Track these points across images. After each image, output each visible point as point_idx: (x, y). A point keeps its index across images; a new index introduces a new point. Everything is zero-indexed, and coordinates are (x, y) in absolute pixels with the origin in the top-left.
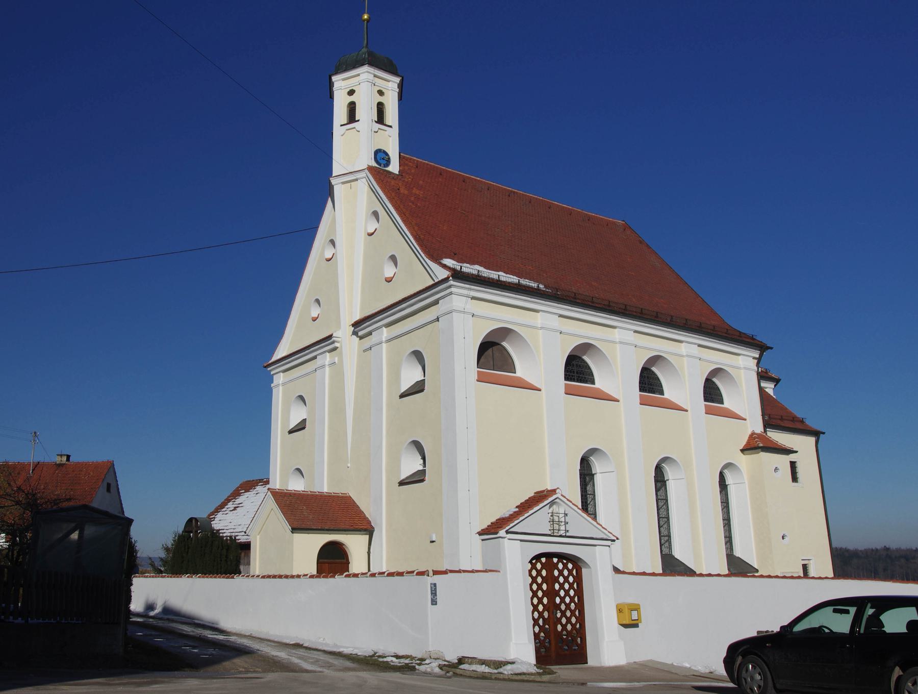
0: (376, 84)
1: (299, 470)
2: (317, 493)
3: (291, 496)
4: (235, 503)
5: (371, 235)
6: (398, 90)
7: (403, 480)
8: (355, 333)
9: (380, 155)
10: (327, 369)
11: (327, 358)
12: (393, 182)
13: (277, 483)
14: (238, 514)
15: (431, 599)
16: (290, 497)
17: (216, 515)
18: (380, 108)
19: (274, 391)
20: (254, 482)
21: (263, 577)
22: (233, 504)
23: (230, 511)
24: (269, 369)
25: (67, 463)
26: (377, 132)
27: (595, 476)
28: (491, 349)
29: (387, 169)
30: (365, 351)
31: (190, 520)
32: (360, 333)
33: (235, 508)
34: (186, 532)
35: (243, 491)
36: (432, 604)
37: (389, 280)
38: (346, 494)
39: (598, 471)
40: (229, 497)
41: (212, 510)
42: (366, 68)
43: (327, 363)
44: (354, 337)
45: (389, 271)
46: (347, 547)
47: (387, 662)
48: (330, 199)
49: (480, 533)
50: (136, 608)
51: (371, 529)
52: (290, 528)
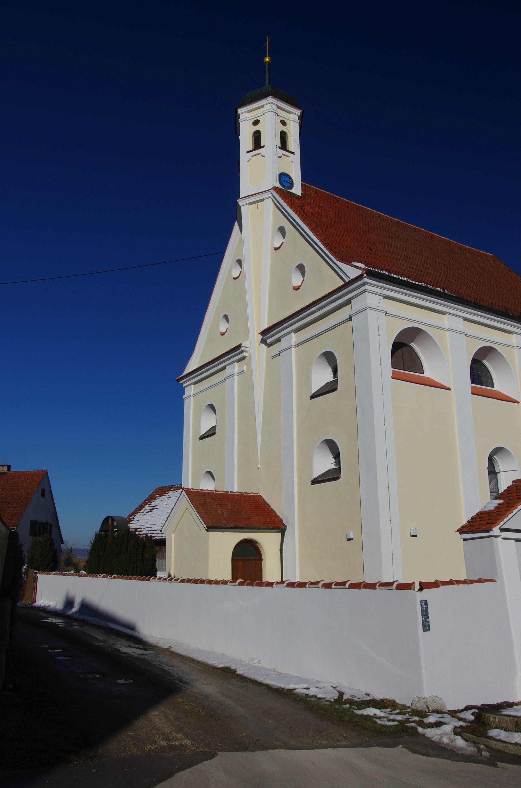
0: (279, 115)
1: (209, 473)
2: (230, 493)
3: (204, 495)
4: (151, 506)
5: (276, 249)
6: (298, 121)
7: (316, 478)
8: (263, 341)
9: (283, 178)
10: (236, 378)
11: (236, 368)
12: (297, 201)
13: (189, 483)
14: (153, 515)
15: (423, 622)
16: (204, 497)
17: (135, 516)
18: (283, 136)
19: (186, 402)
20: (166, 488)
21: (183, 581)
22: (149, 506)
23: (147, 512)
24: (181, 382)
25: (8, 472)
26: (280, 157)
27: (498, 475)
28: (401, 349)
29: (290, 191)
30: (273, 357)
31: (107, 519)
32: (268, 341)
33: (151, 510)
34: (104, 531)
35: (158, 496)
36: (424, 630)
37: (296, 288)
38: (257, 494)
39: (501, 470)
40: (145, 500)
41: (132, 511)
42: (270, 99)
43: (236, 372)
44: (263, 345)
45: (296, 280)
46: (260, 545)
47: (368, 716)
48: (236, 223)
49: (462, 531)
50: (56, 605)
51: (284, 527)
52: (205, 526)
